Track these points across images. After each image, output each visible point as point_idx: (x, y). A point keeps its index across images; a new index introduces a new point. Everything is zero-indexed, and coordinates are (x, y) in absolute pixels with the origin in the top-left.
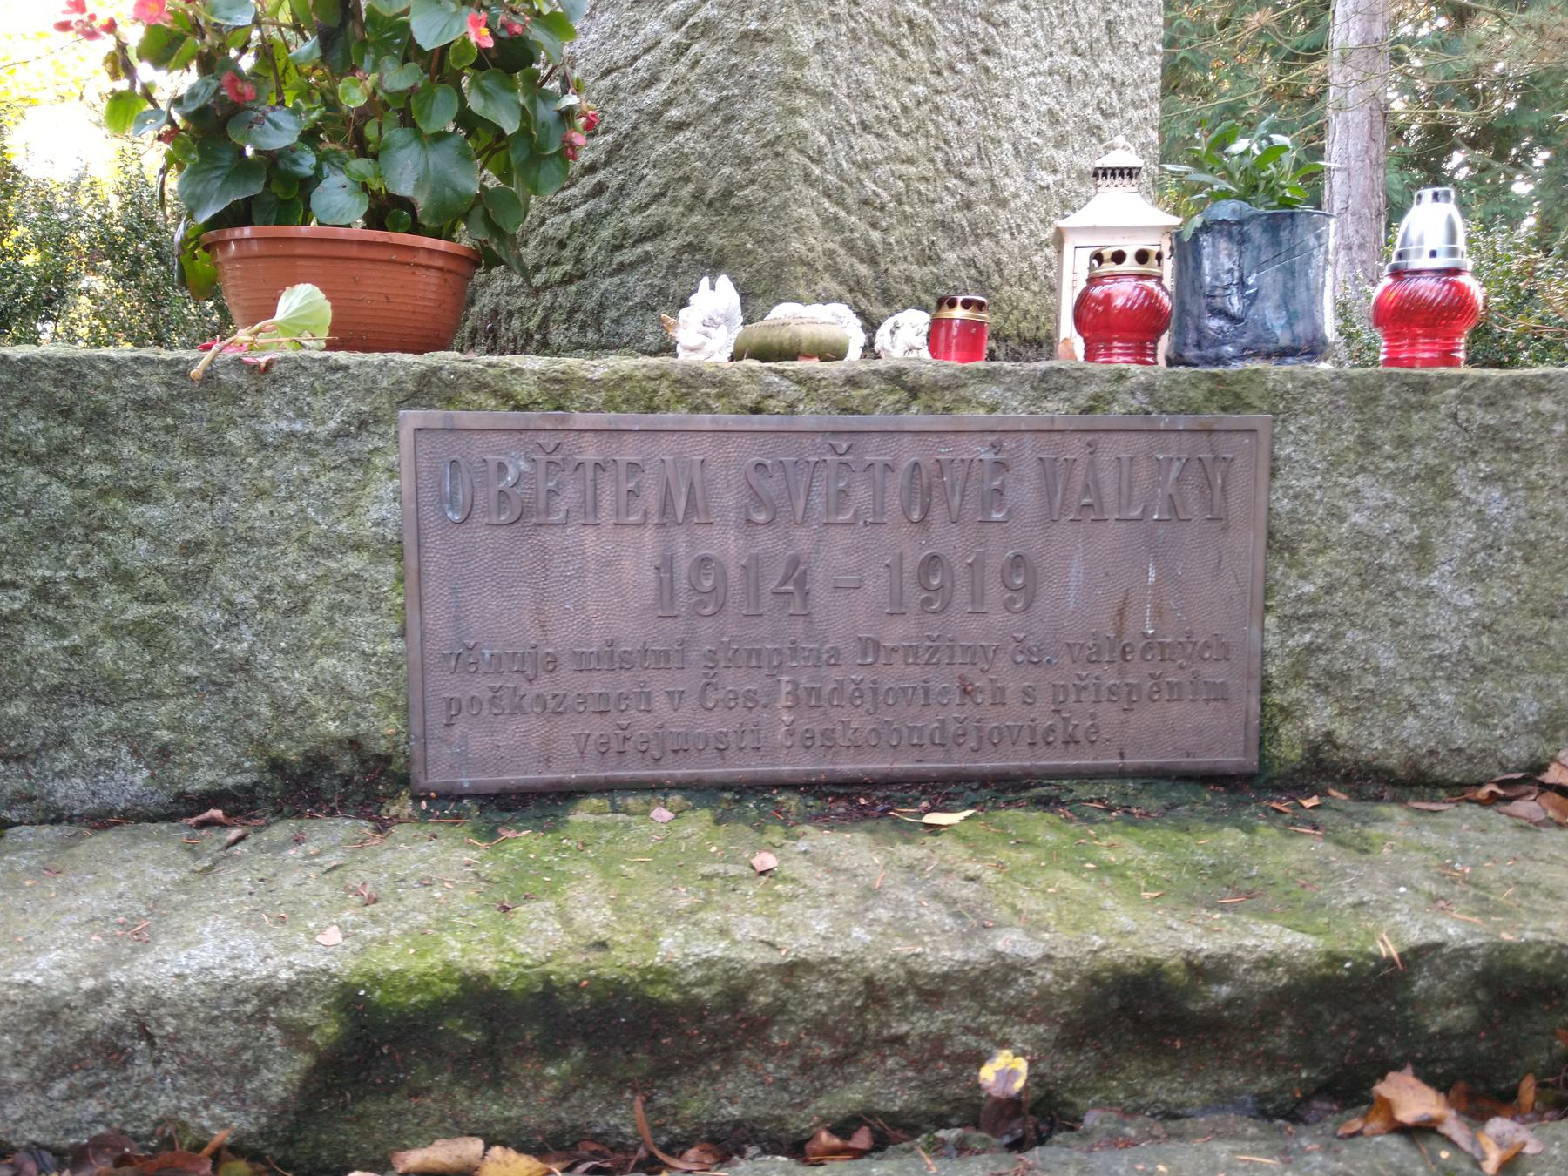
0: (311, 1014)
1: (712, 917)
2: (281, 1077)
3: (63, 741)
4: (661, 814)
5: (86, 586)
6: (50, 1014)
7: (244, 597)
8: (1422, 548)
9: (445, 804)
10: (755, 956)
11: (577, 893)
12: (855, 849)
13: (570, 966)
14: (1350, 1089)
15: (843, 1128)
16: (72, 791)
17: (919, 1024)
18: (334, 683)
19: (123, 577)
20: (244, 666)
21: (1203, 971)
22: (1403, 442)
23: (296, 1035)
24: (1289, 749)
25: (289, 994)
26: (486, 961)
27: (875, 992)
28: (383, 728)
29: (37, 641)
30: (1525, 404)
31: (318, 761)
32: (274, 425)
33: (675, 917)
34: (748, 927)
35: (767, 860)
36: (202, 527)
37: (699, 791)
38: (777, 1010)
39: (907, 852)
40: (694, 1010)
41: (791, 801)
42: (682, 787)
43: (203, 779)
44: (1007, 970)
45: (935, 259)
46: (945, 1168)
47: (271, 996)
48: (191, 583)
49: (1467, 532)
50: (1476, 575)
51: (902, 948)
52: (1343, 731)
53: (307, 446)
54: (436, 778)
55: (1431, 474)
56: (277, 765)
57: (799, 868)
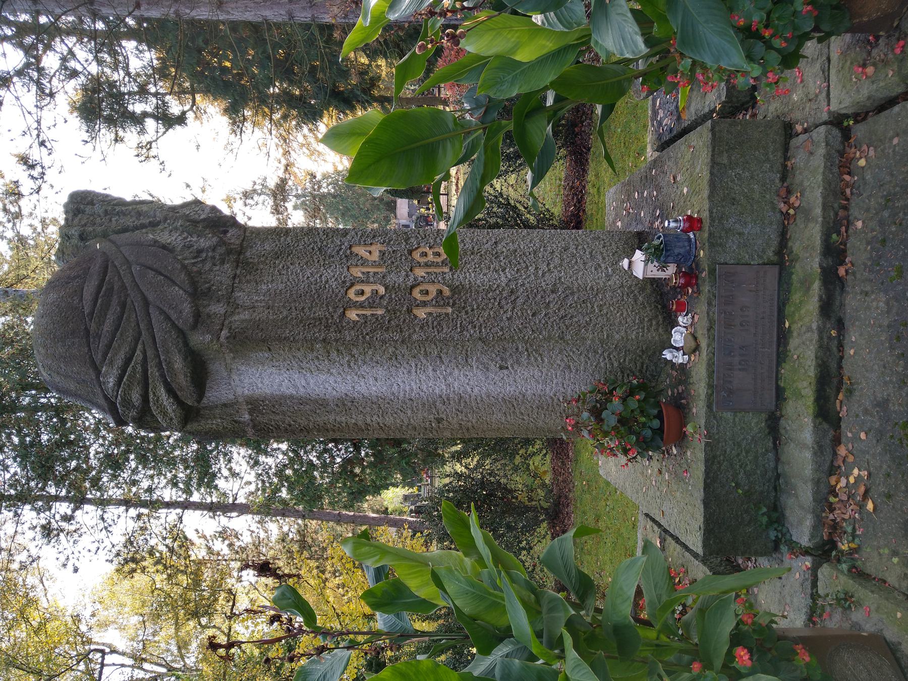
0: (818, 421)
1: (806, 367)
2: (826, 426)
3: (764, 465)
4: (783, 371)
5: (740, 461)
6: (815, 454)
7: (742, 437)
8: (740, 234)
9: (778, 406)
10: (814, 363)
11: (800, 386)
12: (793, 343)
13: (813, 387)
14: (841, 282)
15: (840, 351)
16: (772, 464)
17: (825, 340)
18: (756, 423)
19: (738, 455)
20: (753, 437)
21: (821, 299)
22: (720, 237)
23: (820, 424)
24: (775, 259)
25: (815, 424)
26: (812, 399)
27: (820, 347)
28: (764, 416)
29: (748, 468)
30: (714, 215)
31: (769, 427)
32: (715, 431)
33: (806, 372)
34: (809, 363)
35: (795, 357)
36: (731, 442)
37: (778, 364)
38: (823, 361)
39: (795, 334)
40: (821, 371)
41: (781, 349)
42: (777, 368)
43: (771, 445)
44: (819, 328)
45: (643, 303)
46: (855, 218)
47: (815, 427)
48: (739, 445)
49: (737, 226)
50: (745, 224)
51: (814, 342)
52: (772, 249)
53: (718, 426)
54: (773, 408)
55: (726, 233)
56: (769, 433)
57: (797, 352)
